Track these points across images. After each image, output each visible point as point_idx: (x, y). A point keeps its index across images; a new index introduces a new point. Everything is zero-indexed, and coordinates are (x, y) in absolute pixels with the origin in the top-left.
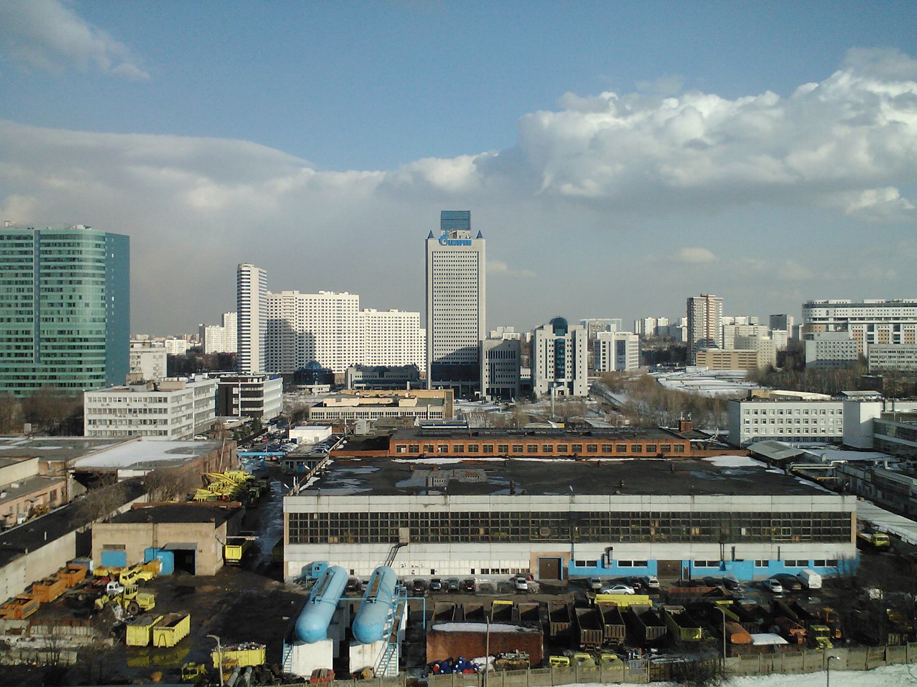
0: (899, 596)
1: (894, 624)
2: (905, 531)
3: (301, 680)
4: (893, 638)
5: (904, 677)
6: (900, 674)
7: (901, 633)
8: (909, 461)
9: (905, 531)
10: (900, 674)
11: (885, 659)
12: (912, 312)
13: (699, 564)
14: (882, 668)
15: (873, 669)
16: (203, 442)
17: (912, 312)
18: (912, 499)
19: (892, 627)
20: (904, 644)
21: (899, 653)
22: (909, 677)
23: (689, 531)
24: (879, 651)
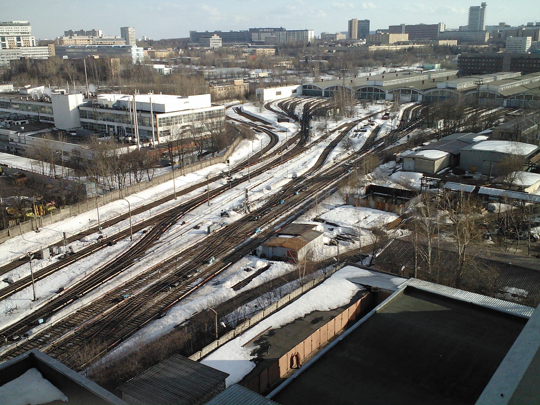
0: (11, 199)
1: (11, 215)
2: (10, 162)
3: (63, 402)
4: (11, 223)
5: (21, 242)
6: (18, 241)
7: (15, 219)
8: (6, 121)
9: (10, 162)
10: (18, 241)
11: (9, 235)
12: (26, 29)
13: (69, 33)
14: (8, 241)
15: (3, 242)
16: (125, 396)
17: (26, 29)
18: (10, 143)
19: (10, 217)
20: (18, 224)
21: (17, 230)
22: (24, 241)
23: (537, 66)
24: (5, 232)
